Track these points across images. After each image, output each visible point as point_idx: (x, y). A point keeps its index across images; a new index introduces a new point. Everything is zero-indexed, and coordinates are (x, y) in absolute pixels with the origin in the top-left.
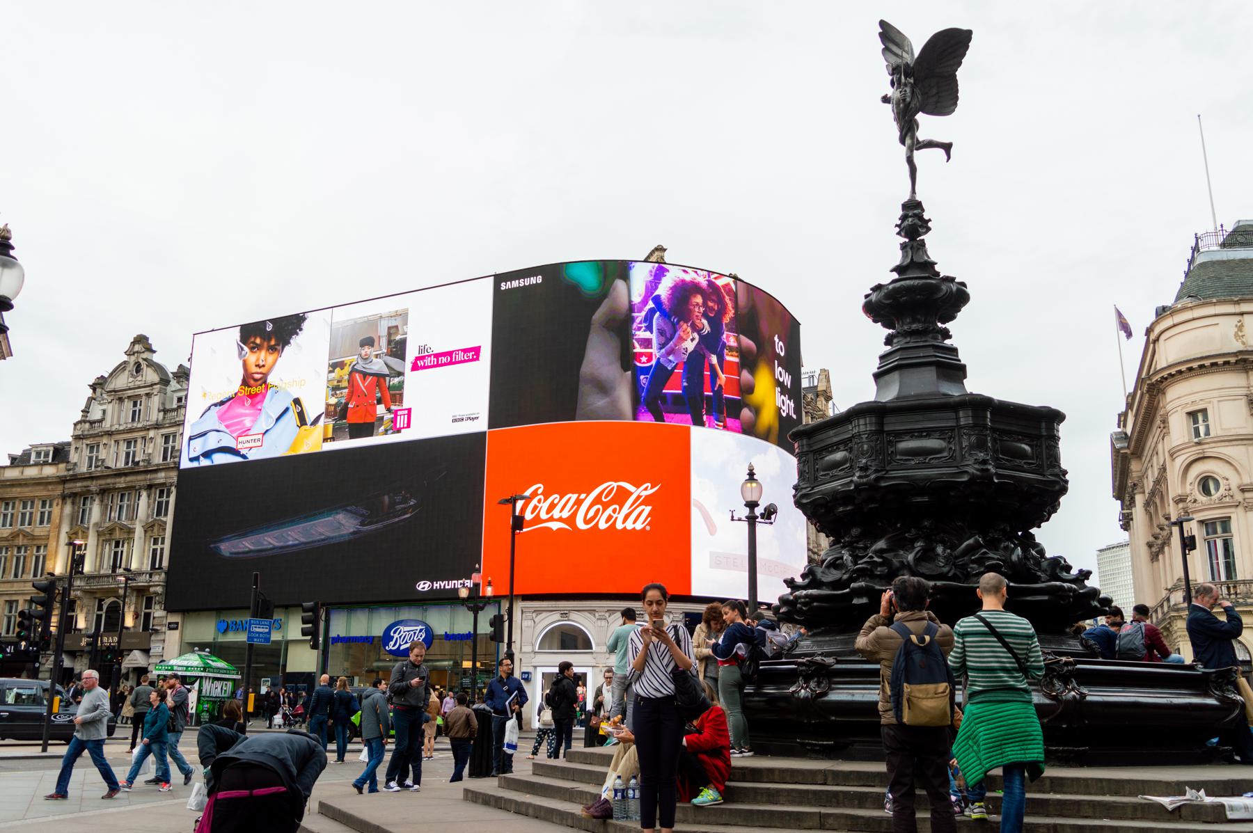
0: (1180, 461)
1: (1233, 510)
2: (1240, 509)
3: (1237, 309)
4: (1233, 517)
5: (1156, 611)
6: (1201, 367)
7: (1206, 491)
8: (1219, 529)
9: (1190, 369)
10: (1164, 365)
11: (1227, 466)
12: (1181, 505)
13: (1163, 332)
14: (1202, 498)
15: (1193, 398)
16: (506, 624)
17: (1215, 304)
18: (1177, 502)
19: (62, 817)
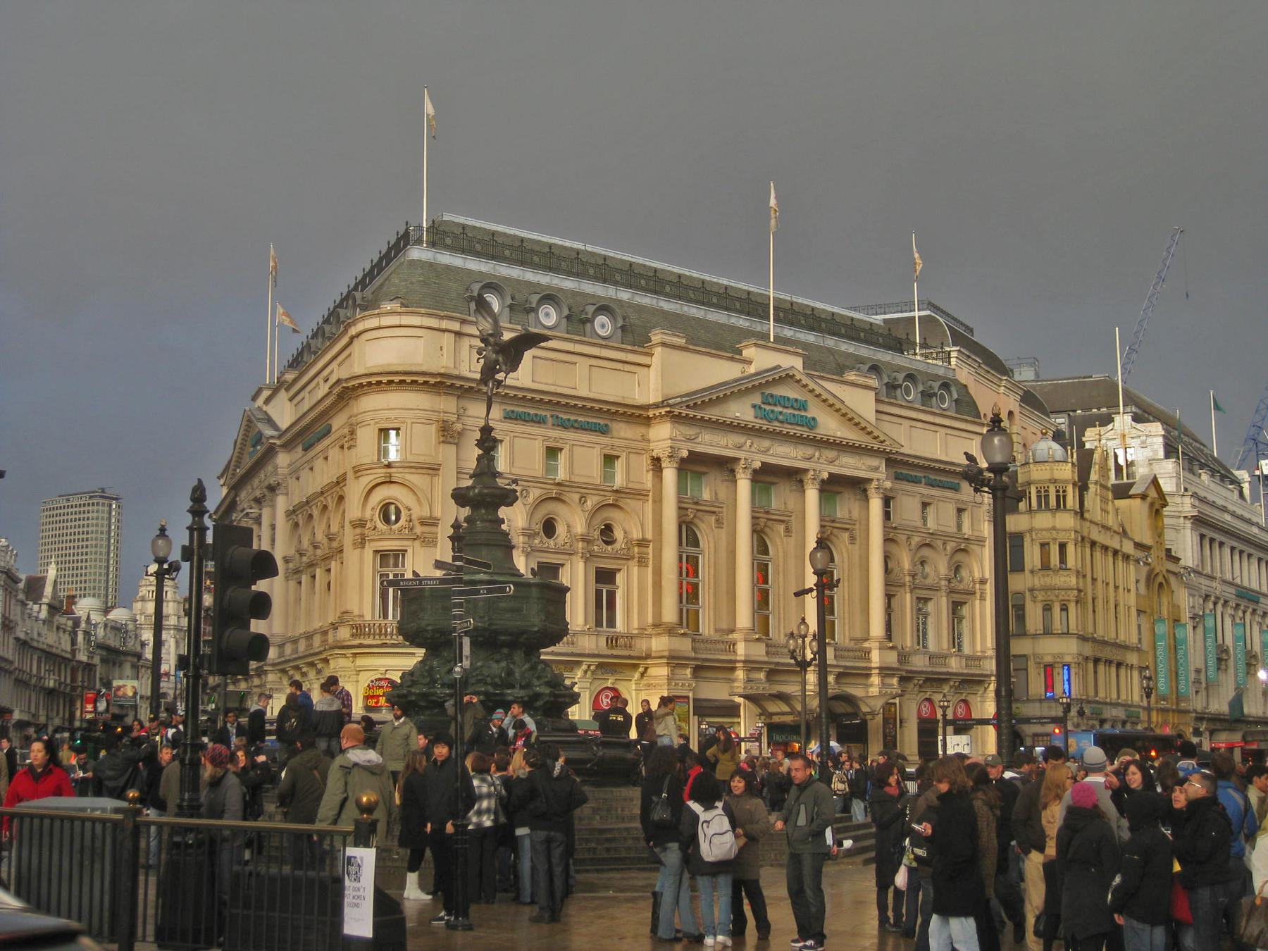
0: (366, 481)
1: (409, 543)
2: (417, 543)
3: (456, 326)
4: (410, 550)
5: (281, 646)
6: (402, 382)
7: (386, 519)
8: (392, 561)
9: (370, 384)
10: (363, 372)
11: (411, 495)
12: (358, 531)
13: (358, 335)
14: (381, 526)
15: (387, 414)
16: (578, 338)
17: (422, 315)
18: (354, 527)
19: (431, 311)
